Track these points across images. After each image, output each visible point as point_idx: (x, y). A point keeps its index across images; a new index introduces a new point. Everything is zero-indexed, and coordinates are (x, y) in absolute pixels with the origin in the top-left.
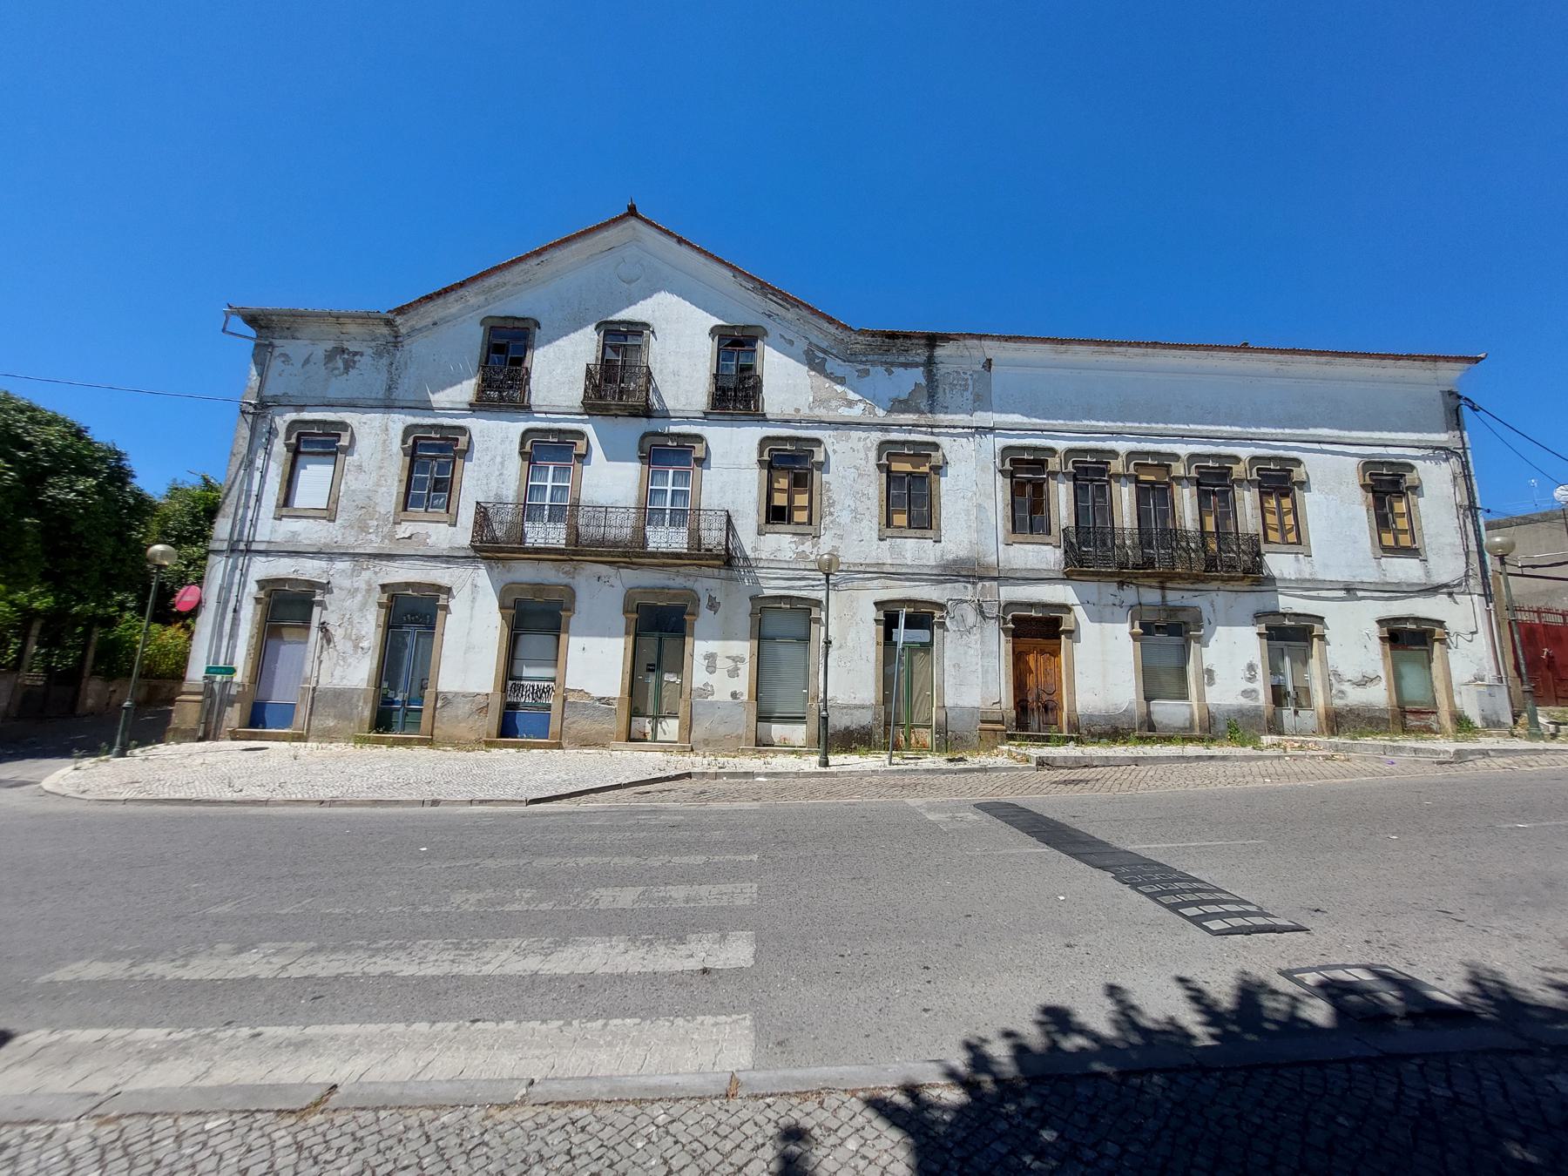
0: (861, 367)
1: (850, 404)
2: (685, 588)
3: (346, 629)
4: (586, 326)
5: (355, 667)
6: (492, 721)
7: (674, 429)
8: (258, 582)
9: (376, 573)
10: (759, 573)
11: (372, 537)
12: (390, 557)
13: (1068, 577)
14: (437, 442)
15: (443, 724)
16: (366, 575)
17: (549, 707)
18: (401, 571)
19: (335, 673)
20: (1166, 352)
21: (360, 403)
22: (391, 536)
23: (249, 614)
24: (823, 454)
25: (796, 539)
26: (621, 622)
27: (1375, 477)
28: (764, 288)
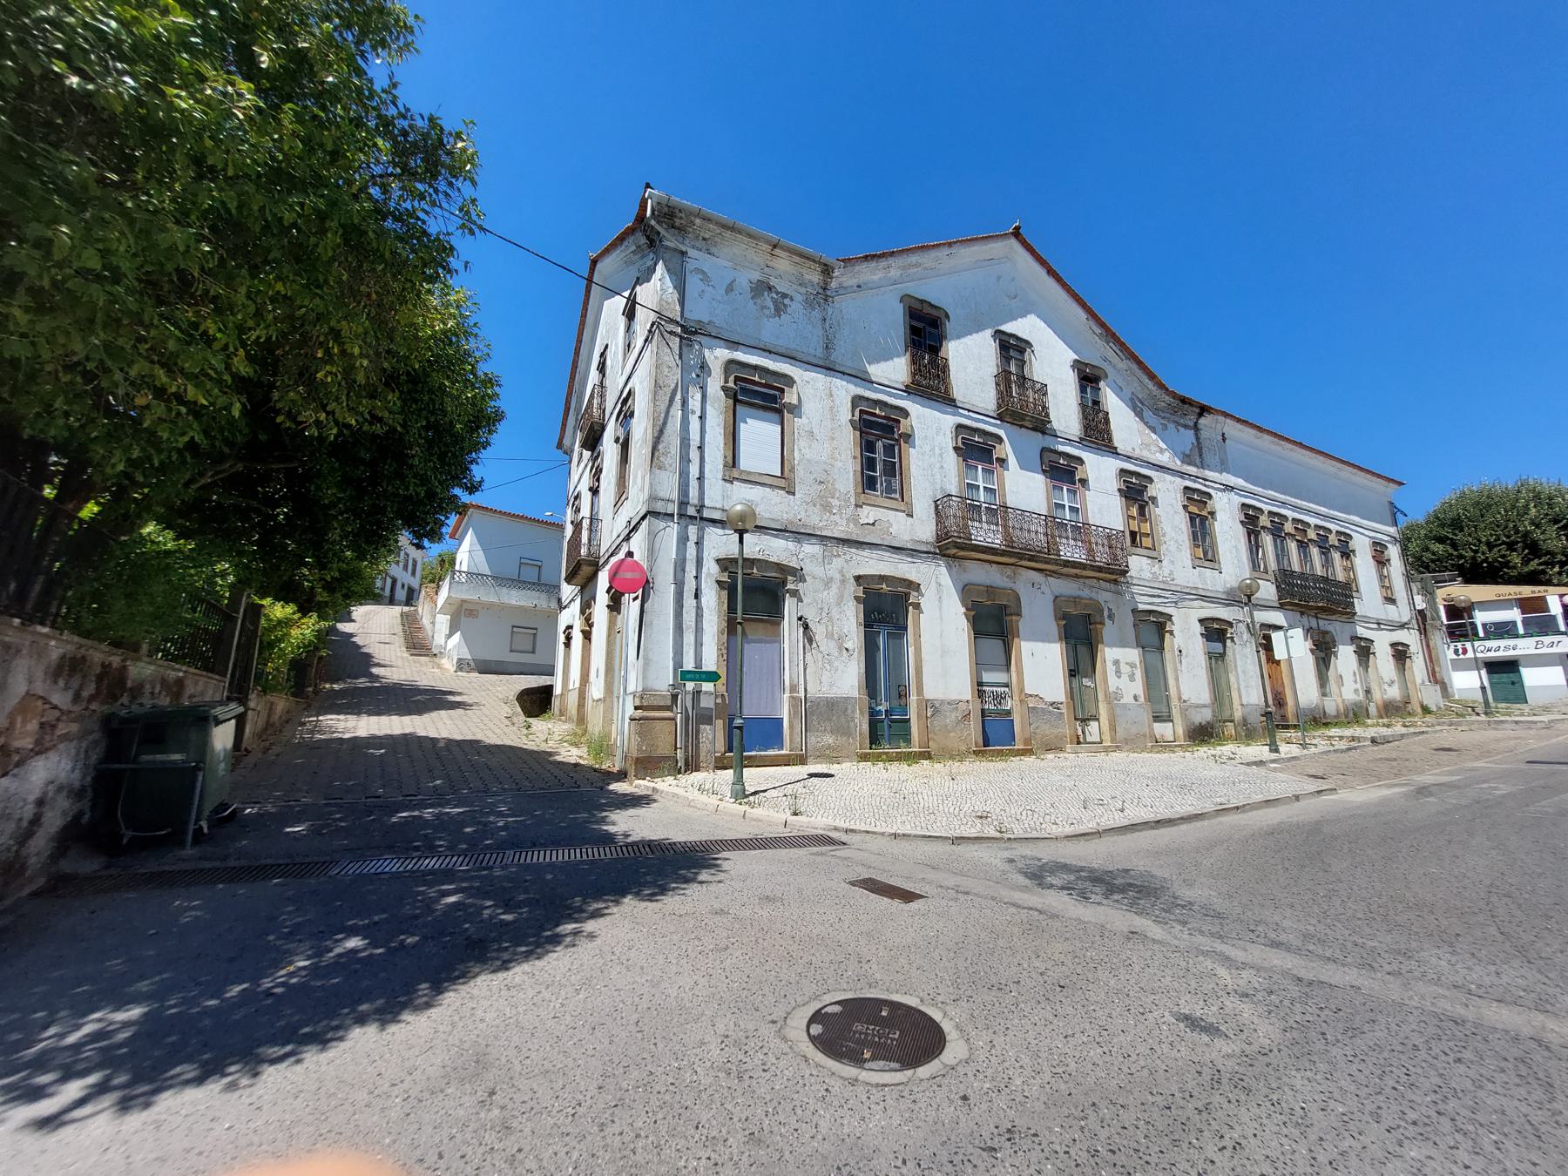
0: (1163, 421)
1: (1162, 451)
2: (1091, 599)
3: (827, 626)
4: (983, 330)
5: (843, 672)
6: (974, 730)
7: (1061, 448)
8: (718, 561)
9: (847, 561)
10: (1135, 589)
11: (836, 518)
12: (859, 544)
13: (1282, 607)
14: (880, 420)
15: (935, 734)
16: (837, 563)
17: (1009, 713)
18: (871, 562)
19: (823, 679)
20: (1304, 452)
21: (799, 357)
22: (854, 520)
23: (712, 599)
24: (795, 396)
25: (1149, 561)
26: (1053, 628)
27: (865, 416)
28: (1110, 335)
